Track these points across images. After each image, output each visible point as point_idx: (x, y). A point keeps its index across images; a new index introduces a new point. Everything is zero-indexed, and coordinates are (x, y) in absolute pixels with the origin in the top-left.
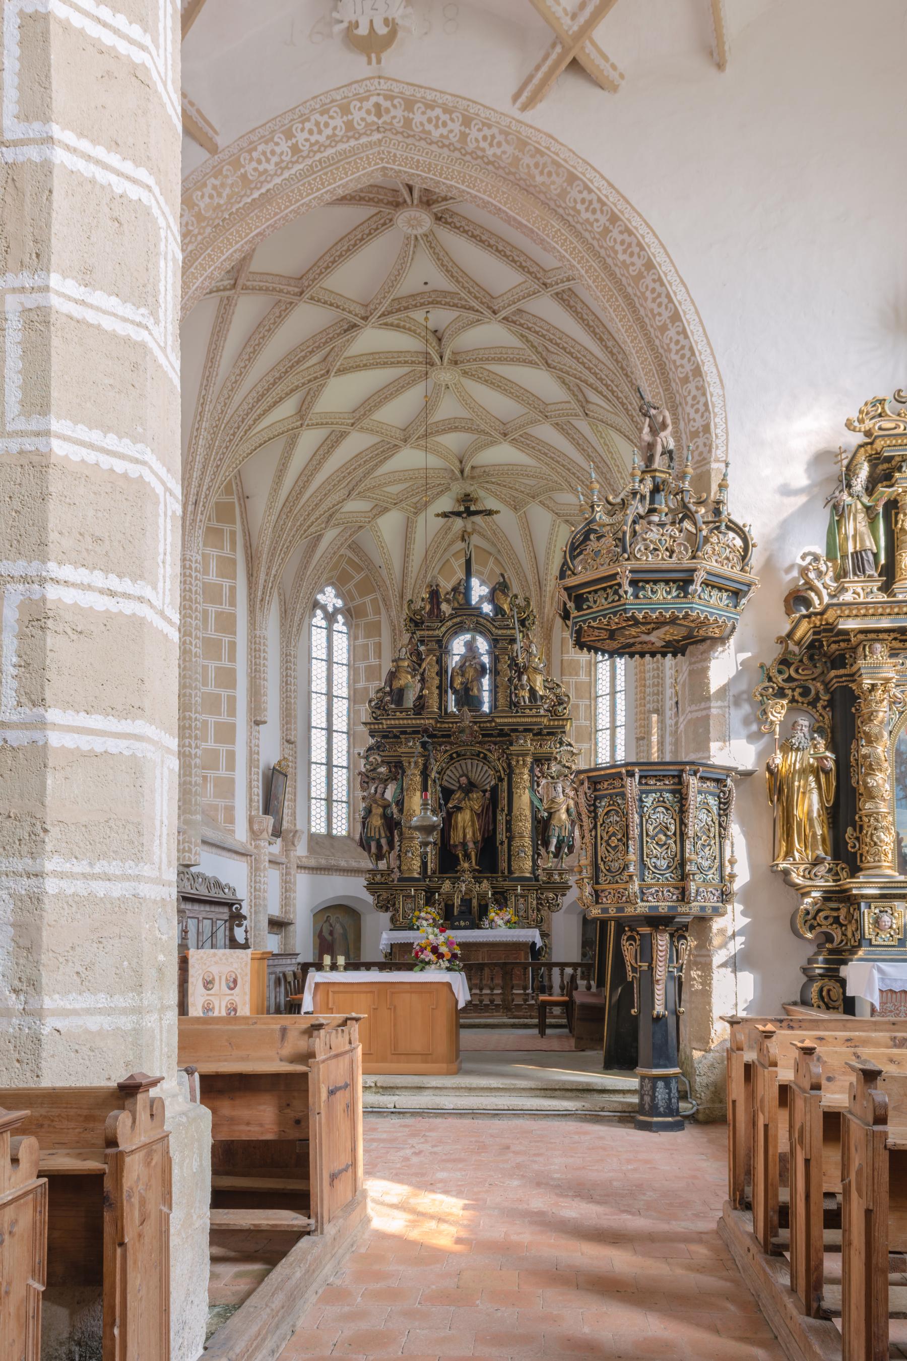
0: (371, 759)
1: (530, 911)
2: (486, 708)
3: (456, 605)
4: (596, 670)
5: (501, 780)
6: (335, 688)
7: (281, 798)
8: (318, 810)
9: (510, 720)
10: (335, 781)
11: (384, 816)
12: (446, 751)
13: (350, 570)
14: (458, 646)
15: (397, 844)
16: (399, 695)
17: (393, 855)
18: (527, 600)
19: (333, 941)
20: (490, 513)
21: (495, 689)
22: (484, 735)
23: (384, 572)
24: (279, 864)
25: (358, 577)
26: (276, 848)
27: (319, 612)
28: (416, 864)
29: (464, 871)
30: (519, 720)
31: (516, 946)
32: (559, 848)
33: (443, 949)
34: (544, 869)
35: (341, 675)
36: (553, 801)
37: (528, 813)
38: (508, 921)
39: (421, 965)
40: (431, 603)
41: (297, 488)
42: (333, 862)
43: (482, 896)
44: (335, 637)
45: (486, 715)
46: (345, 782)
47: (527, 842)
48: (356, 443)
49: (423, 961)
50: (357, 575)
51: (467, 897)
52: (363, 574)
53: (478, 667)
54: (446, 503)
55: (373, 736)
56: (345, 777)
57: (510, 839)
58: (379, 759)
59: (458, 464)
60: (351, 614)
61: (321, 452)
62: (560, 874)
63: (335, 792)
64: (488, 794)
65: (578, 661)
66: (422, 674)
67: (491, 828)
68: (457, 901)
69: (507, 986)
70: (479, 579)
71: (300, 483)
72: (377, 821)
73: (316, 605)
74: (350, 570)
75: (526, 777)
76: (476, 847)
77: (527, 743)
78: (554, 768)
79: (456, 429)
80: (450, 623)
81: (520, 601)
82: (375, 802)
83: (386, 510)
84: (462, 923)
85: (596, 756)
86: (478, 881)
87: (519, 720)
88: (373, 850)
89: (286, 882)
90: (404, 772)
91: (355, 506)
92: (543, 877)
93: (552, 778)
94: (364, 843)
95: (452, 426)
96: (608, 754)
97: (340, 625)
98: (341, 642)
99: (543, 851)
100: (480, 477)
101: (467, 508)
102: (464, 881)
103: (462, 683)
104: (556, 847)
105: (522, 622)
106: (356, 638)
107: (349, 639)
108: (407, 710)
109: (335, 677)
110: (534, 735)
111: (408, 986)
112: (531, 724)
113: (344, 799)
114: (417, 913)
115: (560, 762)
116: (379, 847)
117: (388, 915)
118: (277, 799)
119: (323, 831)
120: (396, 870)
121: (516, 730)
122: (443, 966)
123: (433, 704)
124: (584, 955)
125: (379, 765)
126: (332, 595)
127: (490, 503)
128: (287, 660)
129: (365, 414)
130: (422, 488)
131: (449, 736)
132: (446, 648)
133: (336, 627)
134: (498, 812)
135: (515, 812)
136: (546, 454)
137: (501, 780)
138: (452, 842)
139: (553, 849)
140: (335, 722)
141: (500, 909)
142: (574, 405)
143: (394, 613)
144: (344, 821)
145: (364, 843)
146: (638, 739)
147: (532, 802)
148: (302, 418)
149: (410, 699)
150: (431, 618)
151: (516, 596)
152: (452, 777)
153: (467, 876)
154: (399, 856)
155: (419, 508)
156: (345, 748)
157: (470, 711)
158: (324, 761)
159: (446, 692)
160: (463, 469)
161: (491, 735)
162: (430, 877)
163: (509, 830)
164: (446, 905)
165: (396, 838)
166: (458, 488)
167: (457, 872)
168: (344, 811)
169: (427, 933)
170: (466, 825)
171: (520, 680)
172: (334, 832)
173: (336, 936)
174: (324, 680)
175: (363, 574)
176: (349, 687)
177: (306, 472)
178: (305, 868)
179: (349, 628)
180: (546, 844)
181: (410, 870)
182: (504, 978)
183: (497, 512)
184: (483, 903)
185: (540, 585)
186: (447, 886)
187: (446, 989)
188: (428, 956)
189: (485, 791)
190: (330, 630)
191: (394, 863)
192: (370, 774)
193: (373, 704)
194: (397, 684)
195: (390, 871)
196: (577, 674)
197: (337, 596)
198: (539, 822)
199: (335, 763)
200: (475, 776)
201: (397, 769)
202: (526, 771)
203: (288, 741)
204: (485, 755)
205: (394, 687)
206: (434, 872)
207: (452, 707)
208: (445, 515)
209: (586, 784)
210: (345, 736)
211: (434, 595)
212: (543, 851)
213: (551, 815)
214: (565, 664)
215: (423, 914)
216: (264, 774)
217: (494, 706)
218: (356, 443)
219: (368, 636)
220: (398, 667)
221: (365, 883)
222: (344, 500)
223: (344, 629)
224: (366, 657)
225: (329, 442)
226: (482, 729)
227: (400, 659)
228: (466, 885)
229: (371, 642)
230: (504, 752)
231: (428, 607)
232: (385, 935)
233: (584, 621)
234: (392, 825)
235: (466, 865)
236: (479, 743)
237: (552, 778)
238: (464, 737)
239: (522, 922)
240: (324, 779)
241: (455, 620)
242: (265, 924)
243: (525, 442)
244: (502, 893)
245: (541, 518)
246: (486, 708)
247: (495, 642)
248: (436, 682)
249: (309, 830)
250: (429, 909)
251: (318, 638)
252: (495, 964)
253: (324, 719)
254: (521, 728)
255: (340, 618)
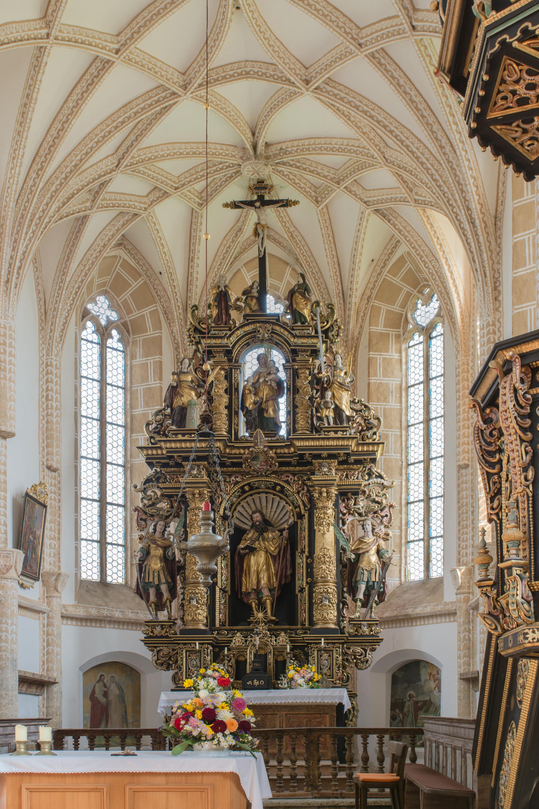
0: (149, 493)
1: (335, 668)
2: (283, 432)
3: (248, 311)
4: (407, 395)
5: (300, 516)
6: (109, 414)
7: (39, 533)
8: (89, 553)
9: (312, 443)
10: (109, 521)
11: (165, 559)
12: (237, 483)
13: (125, 275)
14: (250, 363)
15: (179, 591)
16: (180, 415)
17: (175, 604)
18: (330, 307)
19: (108, 704)
20: (286, 203)
21: (293, 412)
22: (281, 464)
23: (165, 278)
24: (39, 612)
25: (135, 285)
26: (35, 593)
27: (89, 324)
28: (202, 614)
29: (258, 623)
30: (322, 443)
31: (318, 709)
32: (368, 595)
33: (225, 715)
34: (351, 620)
35: (116, 399)
36: (361, 541)
37: (332, 553)
38: (311, 680)
39: (186, 742)
40: (219, 307)
41: (49, 138)
42: (105, 613)
43: (279, 651)
44: (109, 355)
45: (282, 440)
46: (121, 523)
47: (332, 588)
48: (121, 86)
49: (188, 736)
50: (129, 274)
51: (262, 652)
52: (140, 281)
53: (274, 384)
54: (237, 191)
55: (151, 465)
56: (121, 516)
57: (312, 585)
58: (159, 493)
59: (250, 135)
60: (128, 330)
61: (78, 90)
62: (369, 626)
63: (109, 533)
64: (285, 533)
65: (387, 385)
66: (209, 393)
67: (289, 572)
68: (250, 657)
69: (312, 757)
70: (274, 296)
71: (53, 132)
72: (156, 565)
73: (85, 314)
74: (125, 275)
75: (330, 512)
76: (272, 596)
77: (330, 472)
78: (362, 503)
79: (247, 75)
80: (240, 332)
81: (323, 309)
82: (154, 542)
83: (166, 195)
84: (256, 683)
85: (408, 494)
86: (274, 633)
87: (322, 443)
88: (152, 598)
89: (48, 634)
90: (187, 506)
91: (127, 185)
92: (349, 629)
93: (360, 515)
94: (141, 591)
95: (242, 71)
96: (422, 491)
97: (114, 342)
98: (116, 361)
99: (349, 599)
100: (275, 155)
101: (261, 196)
102: (258, 634)
103: (255, 403)
104: (364, 595)
105: (326, 332)
106: (133, 357)
107: (125, 358)
108: (190, 432)
109: (109, 401)
110: (340, 463)
111: (162, 780)
112: (337, 448)
113: (121, 542)
114: (202, 671)
115: (369, 496)
116: (159, 594)
117: (171, 673)
118: (34, 533)
119: (96, 577)
120: (179, 622)
121: (318, 457)
122: (225, 744)
123: (221, 423)
124: (393, 718)
125: (158, 500)
126: (105, 306)
127: (285, 192)
128: (47, 369)
129: (132, 38)
130: (210, 174)
131: (240, 465)
132: (236, 361)
133: (109, 342)
134: (298, 554)
135: (318, 552)
136: (357, 107)
137: (300, 516)
138: (244, 589)
139: (360, 596)
140: (109, 453)
141: (301, 666)
142: (403, 19)
143: (176, 328)
144: (120, 567)
145: (141, 591)
146: (461, 467)
147: (337, 541)
148: (48, 25)
149: (194, 420)
150: (221, 324)
151: (317, 303)
152: (244, 515)
153: (261, 628)
154: (182, 605)
155: (205, 198)
156: (121, 483)
157: (266, 435)
158: (96, 497)
159: (237, 413)
160: (256, 148)
161: (289, 464)
162: (218, 630)
163: (310, 574)
164: (237, 662)
165: (179, 585)
166: (250, 171)
167: (249, 623)
168: (121, 555)
169: (209, 689)
170: (260, 568)
171: (323, 397)
172: (109, 579)
173: (111, 697)
174: (96, 403)
175: (140, 281)
176: (125, 414)
177: (60, 117)
178: (72, 618)
179: (125, 345)
180: (353, 591)
181: (195, 621)
182: (307, 748)
183: (296, 203)
184: (280, 659)
185: (344, 296)
186: (238, 640)
187: (229, 784)
188: (197, 726)
189: (281, 531)
190: (103, 346)
191: (175, 612)
192: (149, 511)
193: (151, 428)
194: (178, 402)
195: (172, 622)
196: (385, 400)
197: (111, 307)
198: (345, 566)
199: (109, 500)
200: (271, 513)
201: (180, 505)
202: (330, 504)
203: (49, 468)
204: (282, 487)
205: (175, 405)
206: (223, 624)
207: (243, 432)
208: (235, 205)
209: (517, 371)
210: (121, 469)
211: (222, 297)
212: (349, 599)
213: (359, 556)
214: (372, 388)
215: (210, 672)
216: (15, 501)
217: (293, 428)
218: (121, 86)
219: (147, 355)
220: (180, 382)
221: (143, 636)
222: (112, 171)
223: (120, 346)
224: (145, 379)
225: (87, 77)
226: (279, 456)
227: (182, 373)
228: (260, 639)
229: (151, 360)
230: (304, 484)
231: (215, 312)
232: (163, 697)
233: (511, 31)
234: (174, 568)
235: (260, 615)
236: (274, 472)
237: (360, 515)
238: (257, 465)
239: (328, 680)
240: (96, 518)
241: (247, 329)
242: (14, 682)
243: (333, 93)
244: (302, 648)
245: (345, 207)
246: (283, 432)
247: (293, 354)
248: (225, 400)
249: (77, 575)
250: (216, 666)
251: (89, 354)
252: (298, 732)
253: (96, 449)
254: (325, 453)
255: (114, 332)
